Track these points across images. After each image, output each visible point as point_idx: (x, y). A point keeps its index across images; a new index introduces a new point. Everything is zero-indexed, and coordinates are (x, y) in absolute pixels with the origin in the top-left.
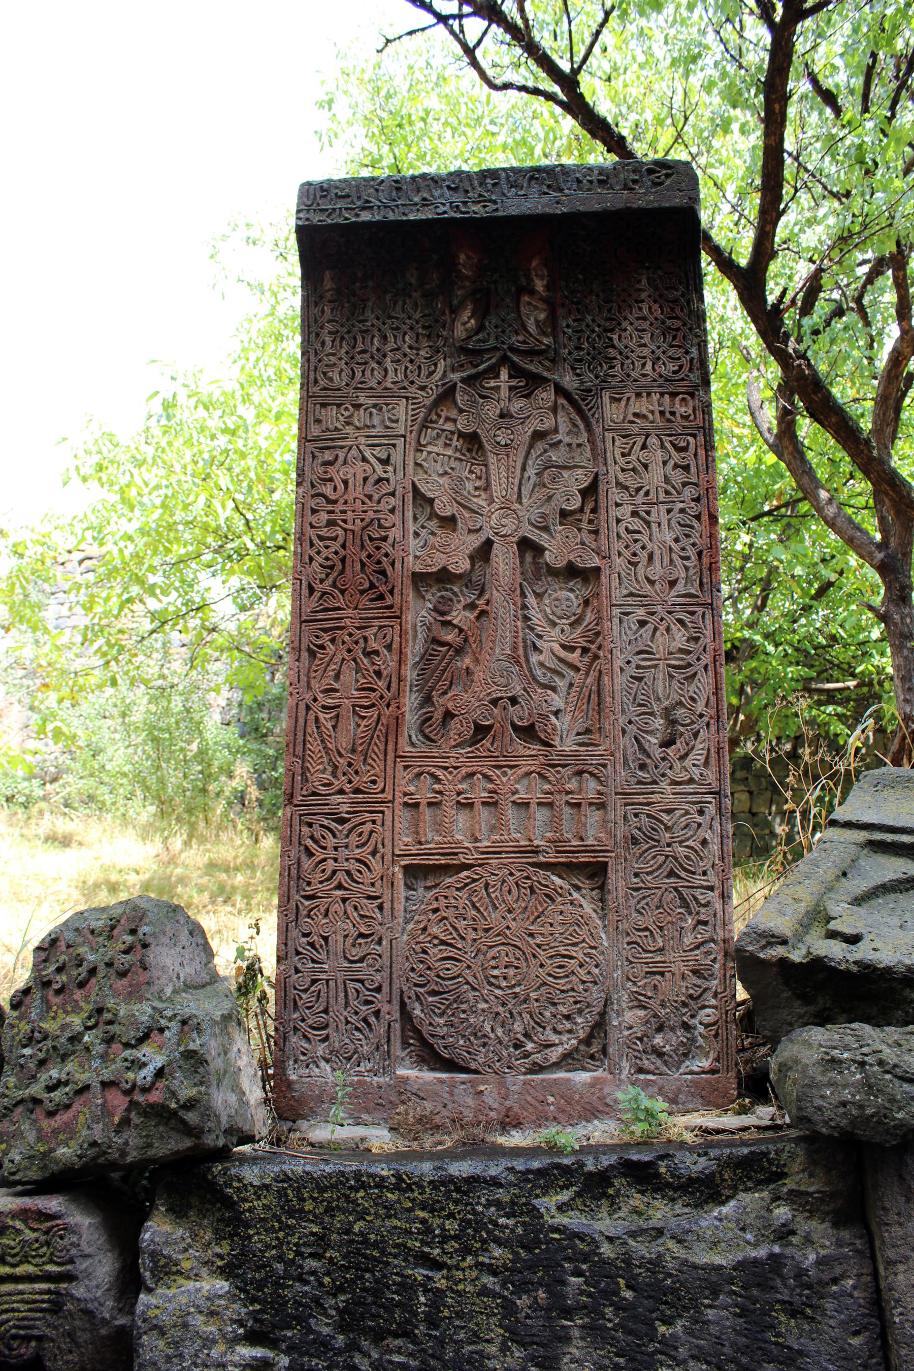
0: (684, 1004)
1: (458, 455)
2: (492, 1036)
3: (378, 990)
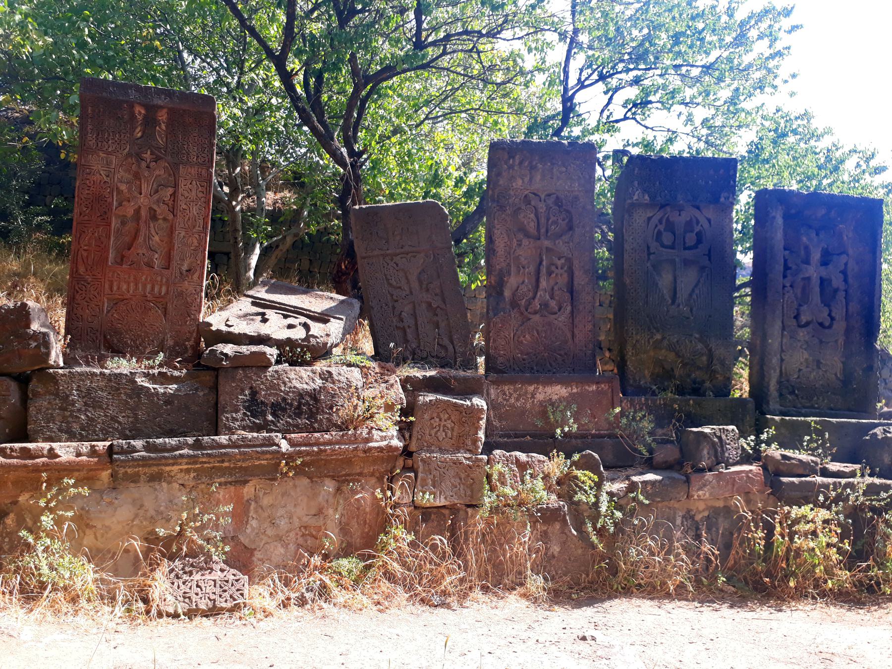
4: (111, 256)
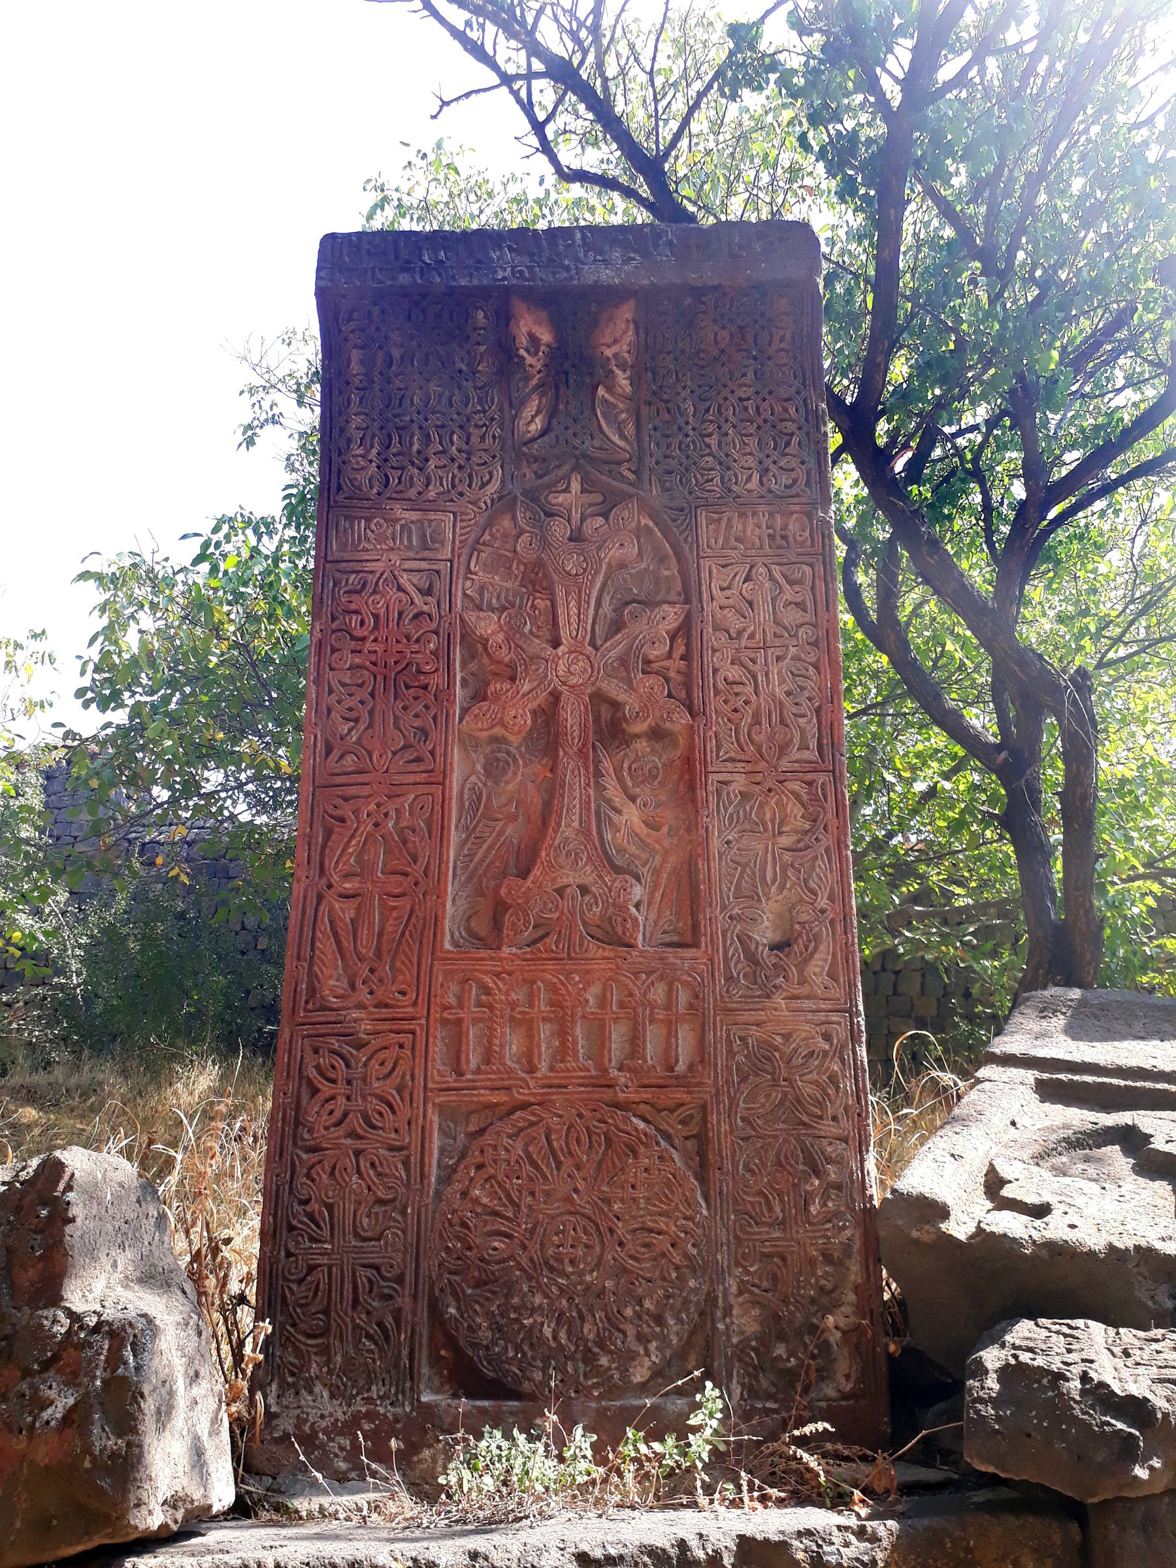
3: (400, 1280)
4: (452, 909)
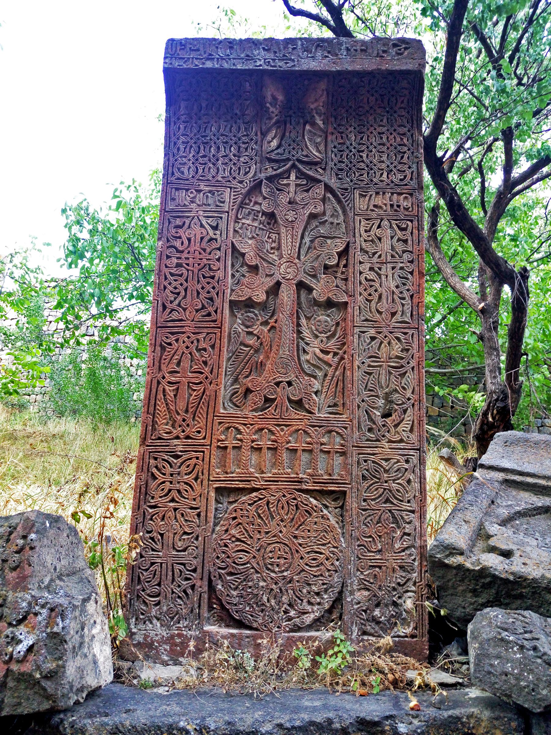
0: (394, 589)
1: (261, 226)
2: (268, 605)
3: (194, 571)
